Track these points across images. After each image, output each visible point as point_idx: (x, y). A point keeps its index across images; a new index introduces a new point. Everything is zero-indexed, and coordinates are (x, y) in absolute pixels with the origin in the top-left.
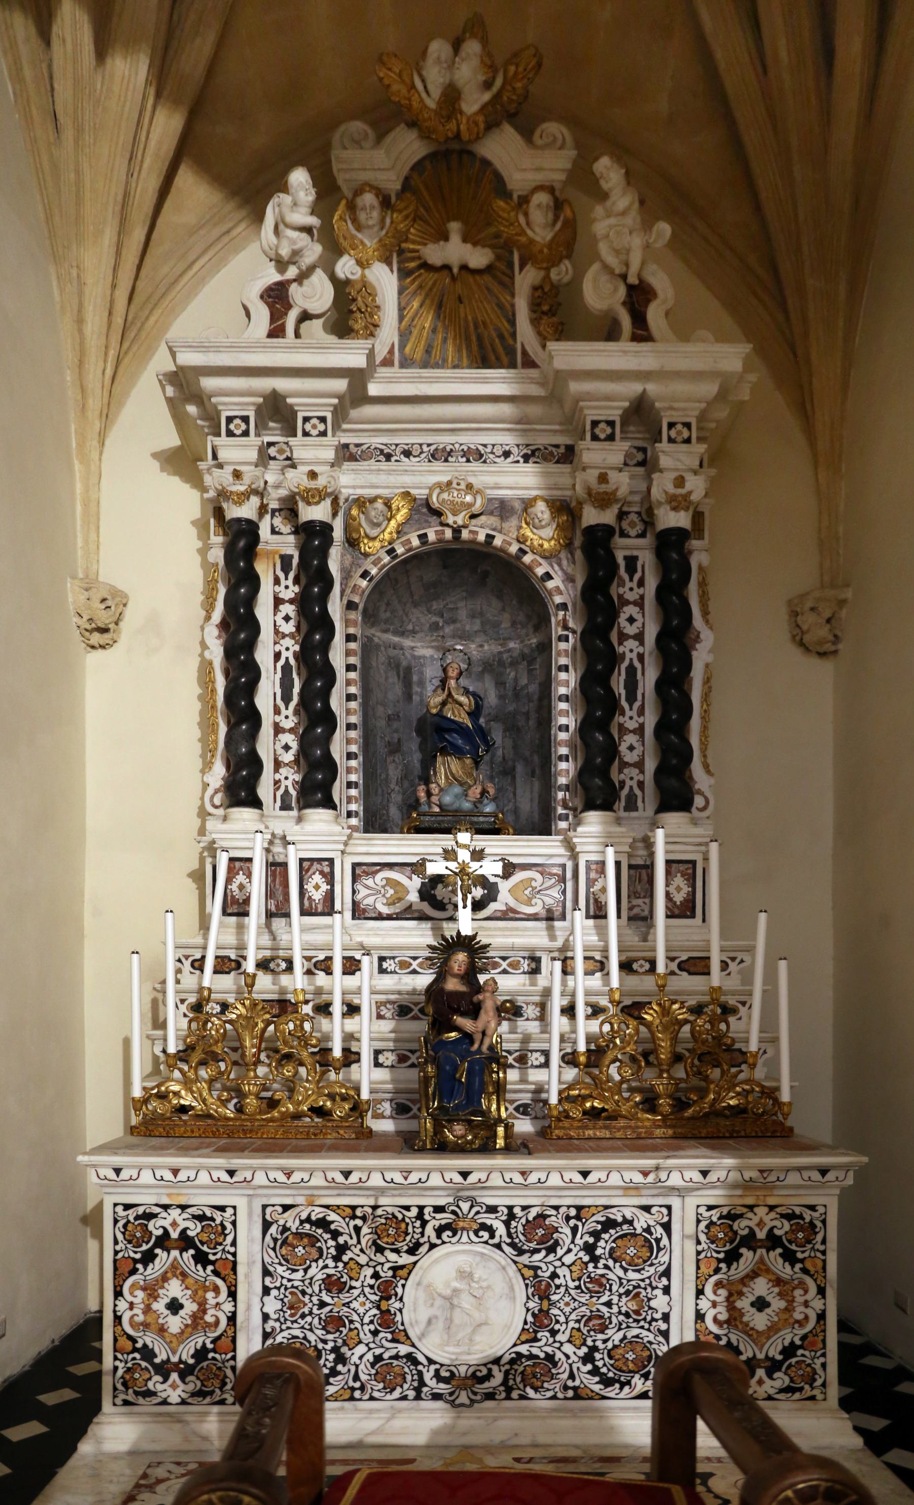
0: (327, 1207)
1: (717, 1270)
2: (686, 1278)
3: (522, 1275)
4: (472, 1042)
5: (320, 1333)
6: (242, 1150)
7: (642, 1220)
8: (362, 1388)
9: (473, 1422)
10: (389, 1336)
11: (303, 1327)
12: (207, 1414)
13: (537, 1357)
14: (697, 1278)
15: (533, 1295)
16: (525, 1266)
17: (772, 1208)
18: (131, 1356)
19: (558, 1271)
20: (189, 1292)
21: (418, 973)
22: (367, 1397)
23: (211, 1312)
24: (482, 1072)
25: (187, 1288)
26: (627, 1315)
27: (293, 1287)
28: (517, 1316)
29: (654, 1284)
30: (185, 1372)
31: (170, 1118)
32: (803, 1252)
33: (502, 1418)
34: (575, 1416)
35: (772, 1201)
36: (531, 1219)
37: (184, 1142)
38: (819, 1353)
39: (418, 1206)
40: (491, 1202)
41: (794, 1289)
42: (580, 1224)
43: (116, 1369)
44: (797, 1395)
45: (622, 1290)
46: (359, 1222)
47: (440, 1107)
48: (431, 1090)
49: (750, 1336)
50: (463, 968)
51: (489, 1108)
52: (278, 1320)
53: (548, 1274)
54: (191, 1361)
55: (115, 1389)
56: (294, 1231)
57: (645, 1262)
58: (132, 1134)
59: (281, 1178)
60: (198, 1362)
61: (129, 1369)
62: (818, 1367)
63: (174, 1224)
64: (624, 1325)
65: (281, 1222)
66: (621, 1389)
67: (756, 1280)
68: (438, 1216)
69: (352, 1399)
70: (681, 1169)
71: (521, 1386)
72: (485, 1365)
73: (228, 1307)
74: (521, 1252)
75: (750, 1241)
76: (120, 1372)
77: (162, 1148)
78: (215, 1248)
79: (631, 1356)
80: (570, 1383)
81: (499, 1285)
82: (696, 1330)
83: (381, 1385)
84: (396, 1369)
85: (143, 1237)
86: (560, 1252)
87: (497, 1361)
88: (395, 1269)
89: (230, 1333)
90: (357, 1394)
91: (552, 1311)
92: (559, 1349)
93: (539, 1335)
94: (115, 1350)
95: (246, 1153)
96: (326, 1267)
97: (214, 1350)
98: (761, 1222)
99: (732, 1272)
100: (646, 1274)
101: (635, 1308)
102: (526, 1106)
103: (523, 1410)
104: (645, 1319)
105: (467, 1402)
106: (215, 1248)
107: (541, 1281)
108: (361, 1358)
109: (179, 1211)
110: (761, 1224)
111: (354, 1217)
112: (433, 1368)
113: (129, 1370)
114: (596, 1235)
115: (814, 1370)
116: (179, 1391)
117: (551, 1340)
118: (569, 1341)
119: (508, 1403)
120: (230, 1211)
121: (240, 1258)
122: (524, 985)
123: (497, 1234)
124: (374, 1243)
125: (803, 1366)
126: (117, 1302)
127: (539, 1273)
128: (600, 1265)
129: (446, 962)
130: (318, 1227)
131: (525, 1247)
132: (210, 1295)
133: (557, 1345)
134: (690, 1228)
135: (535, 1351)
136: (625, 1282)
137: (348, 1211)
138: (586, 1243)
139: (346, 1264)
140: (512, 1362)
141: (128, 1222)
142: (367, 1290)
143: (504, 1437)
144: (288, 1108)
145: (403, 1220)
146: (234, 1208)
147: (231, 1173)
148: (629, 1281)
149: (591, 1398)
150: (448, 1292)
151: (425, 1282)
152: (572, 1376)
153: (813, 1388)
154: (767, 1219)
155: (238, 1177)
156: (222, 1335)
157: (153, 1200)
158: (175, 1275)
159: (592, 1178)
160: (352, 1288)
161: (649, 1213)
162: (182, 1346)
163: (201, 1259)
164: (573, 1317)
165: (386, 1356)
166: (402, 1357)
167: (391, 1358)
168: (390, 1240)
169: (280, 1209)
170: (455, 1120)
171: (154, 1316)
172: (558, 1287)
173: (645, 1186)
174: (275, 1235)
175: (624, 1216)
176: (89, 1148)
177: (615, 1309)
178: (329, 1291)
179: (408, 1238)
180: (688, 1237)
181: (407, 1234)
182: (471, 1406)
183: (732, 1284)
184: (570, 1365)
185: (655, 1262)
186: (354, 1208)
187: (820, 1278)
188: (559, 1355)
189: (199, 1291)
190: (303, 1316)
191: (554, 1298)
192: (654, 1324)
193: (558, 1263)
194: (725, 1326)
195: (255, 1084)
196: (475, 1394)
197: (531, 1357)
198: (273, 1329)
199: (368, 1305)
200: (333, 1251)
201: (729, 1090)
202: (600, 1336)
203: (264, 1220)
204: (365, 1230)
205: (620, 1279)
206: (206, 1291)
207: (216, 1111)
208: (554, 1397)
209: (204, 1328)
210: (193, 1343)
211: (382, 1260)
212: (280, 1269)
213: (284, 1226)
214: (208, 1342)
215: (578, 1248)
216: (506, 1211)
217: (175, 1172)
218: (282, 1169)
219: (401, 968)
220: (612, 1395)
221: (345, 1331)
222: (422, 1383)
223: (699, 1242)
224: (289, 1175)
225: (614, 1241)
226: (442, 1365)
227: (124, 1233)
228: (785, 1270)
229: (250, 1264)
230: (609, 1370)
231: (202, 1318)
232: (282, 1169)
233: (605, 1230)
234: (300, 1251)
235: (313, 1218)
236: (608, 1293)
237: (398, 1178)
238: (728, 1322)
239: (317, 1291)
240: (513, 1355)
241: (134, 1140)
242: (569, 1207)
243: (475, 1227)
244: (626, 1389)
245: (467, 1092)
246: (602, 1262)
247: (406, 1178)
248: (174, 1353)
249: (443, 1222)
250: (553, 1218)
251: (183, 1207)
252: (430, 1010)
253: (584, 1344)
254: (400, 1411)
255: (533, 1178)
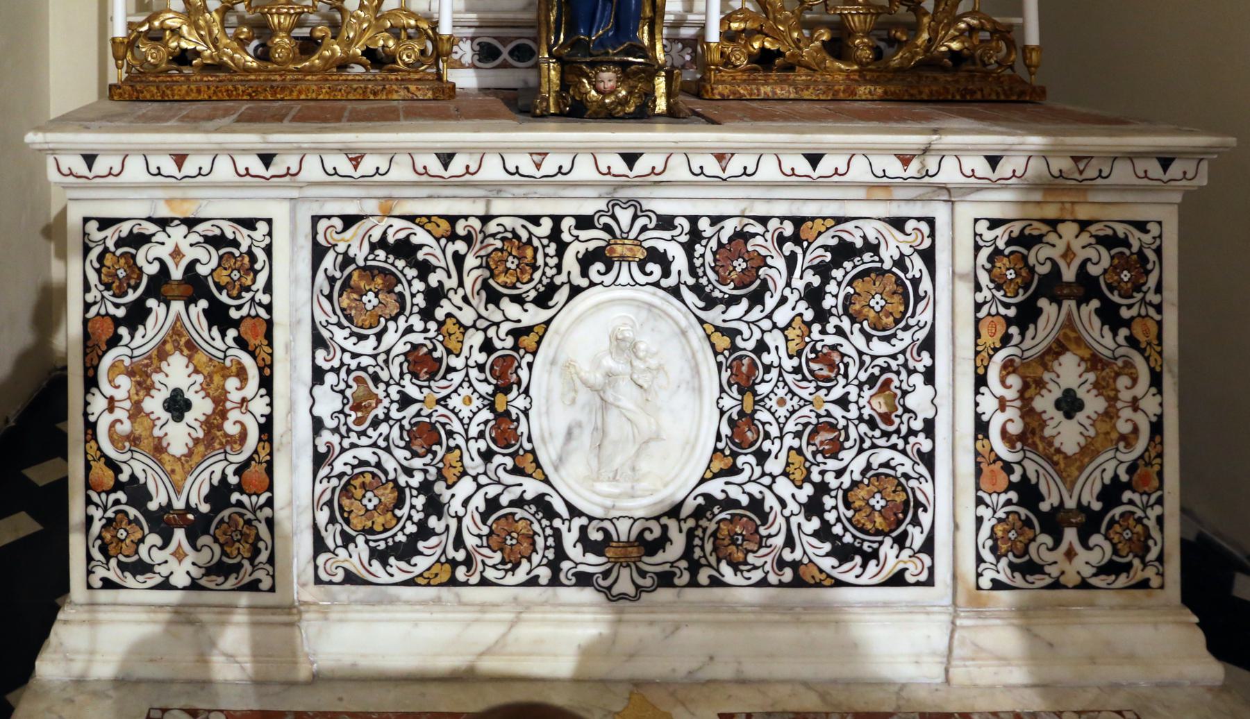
0: (411, 218)
1: (1006, 340)
2: (958, 354)
3: (713, 346)
5: (401, 454)
6: (278, 118)
7: (892, 244)
8: (468, 562)
9: (643, 631)
10: (509, 462)
11: (375, 445)
12: (230, 608)
13: (736, 504)
14: (977, 353)
15: (730, 385)
16: (717, 329)
17: (1084, 225)
18: (113, 497)
19: (768, 338)
20: (199, 378)
22: (475, 579)
23: (234, 415)
25: (196, 371)
26: (872, 424)
27: (359, 368)
28: (705, 423)
29: (911, 364)
30: (197, 527)
31: (166, 71)
32: (1130, 307)
33: (687, 624)
34: (798, 622)
35: (1083, 213)
36: (725, 240)
37: (188, 109)
38: (1154, 498)
39: (552, 217)
40: (664, 208)
41: (1118, 375)
42: (799, 250)
43: (89, 520)
44: (1123, 580)
45: (863, 376)
46: (461, 246)
49: (1054, 464)
52: (336, 430)
53: (751, 344)
54: (205, 508)
55: (89, 558)
56: (361, 263)
57: (897, 322)
58: (111, 97)
59: (345, 167)
60: (215, 510)
61: (110, 521)
62: (1151, 523)
63: (177, 254)
64: (867, 444)
65: (341, 248)
66: (864, 566)
67: (1062, 359)
68: (584, 234)
69: (453, 582)
70: (958, 153)
71: (713, 560)
72: (657, 518)
73: (259, 406)
74: (710, 303)
75: (1051, 286)
76: (96, 527)
77: (158, 119)
78: (239, 297)
79: (878, 502)
80: (788, 556)
81: (677, 366)
82: (977, 454)
83: (498, 557)
84: (521, 524)
85: (128, 277)
86: (770, 302)
87: (674, 511)
88: (517, 333)
89: (263, 454)
90: (461, 573)
91: (758, 416)
92: (770, 487)
93: (740, 460)
94: (88, 486)
95: (286, 123)
96: (410, 330)
97: (239, 488)
98: (1068, 250)
99: (1028, 343)
100: (900, 346)
101: (883, 409)
103: (716, 607)
104: (898, 431)
105: (631, 590)
106: (239, 297)
107: (741, 358)
108: (465, 503)
109: (183, 229)
110: (1068, 253)
111: (453, 237)
112: (578, 522)
113: (110, 521)
114: (823, 270)
115: (1146, 528)
116: (187, 565)
117: (758, 471)
118: (785, 474)
119: (693, 594)
120: (262, 228)
121: (279, 315)
123: (674, 268)
124: (485, 285)
125: (1131, 522)
126: (89, 398)
127: (739, 342)
128: (830, 328)
130: (397, 257)
131: (717, 294)
132: (232, 383)
133: (767, 480)
134: (965, 261)
135: (734, 492)
136: (867, 359)
137: (445, 225)
138: (809, 285)
139: (441, 324)
140: (699, 513)
141: (106, 250)
142: (474, 373)
143: (694, 665)
144: (333, 51)
145: (529, 242)
146: (269, 221)
147: (267, 159)
148: (874, 358)
149: (819, 585)
150: (597, 378)
151: (562, 360)
152: (790, 543)
153: (1145, 565)
154: (1076, 245)
155: (278, 167)
156: (251, 458)
157: (143, 210)
158: (177, 348)
159: (825, 167)
160: (450, 369)
161: (902, 231)
162: (190, 479)
163: (218, 317)
164: (791, 426)
165: (504, 500)
166: (529, 503)
167: (512, 504)
168: (510, 279)
169: (339, 224)
170: (602, 63)
171: (147, 423)
172: (767, 369)
173: (904, 183)
174: (331, 272)
175: (864, 237)
176: (55, 111)
177: (853, 413)
178: (415, 375)
179: (537, 276)
180: (963, 277)
181: (535, 268)
182: (636, 598)
183: (1028, 365)
184: (787, 519)
185: (912, 322)
186: (452, 220)
187: (1155, 356)
188: (770, 502)
189: (216, 373)
190: (375, 424)
191: (762, 389)
192: (912, 440)
193: (766, 324)
194: (1019, 445)
195: (288, 14)
196: (643, 574)
197: (730, 503)
198: (330, 446)
199: (477, 403)
200: (420, 300)
201: (948, 26)
202: (833, 464)
203: (315, 243)
204: (471, 262)
205: (860, 353)
206: (225, 377)
207: (232, 58)
208: (763, 583)
209: (223, 445)
210: (206, 474)
211: (497, 317)
212: (340, 335)
213: (346, 254)
214: (230, 471)
215: (796, 295)
216: (687, 226)
217: (180, 159)
218: (346, 151)
220: (849, 578)
221: (440, 451)
222: (561, 555)
223: (978, 288)
224: (356, 162)
225: (850, 284)
226: (591, 519)
227: (98, 271)
228: (1104, 341)
229: (295, 324)
230: (846, 530)
231: (220, 428)
232: (346, 151)
233: (836, 263)
234: (370, 300)
235: (391, 239)
236: (842, 381)
237: (527, 167)
238: (1022, 437)
239: (397, 377)
240: (700, 500)
241: (116, 107)
242: (782, 219)
243: (641, 255)
244: (872, 566)
246: (834, 321)
247: (538, 166)
248: (178, 492)
249: (592, 246)
250: (759, 240)
251: (191, 223)
253: (807, 479)
254: (528, 607)
255: (735, 167)
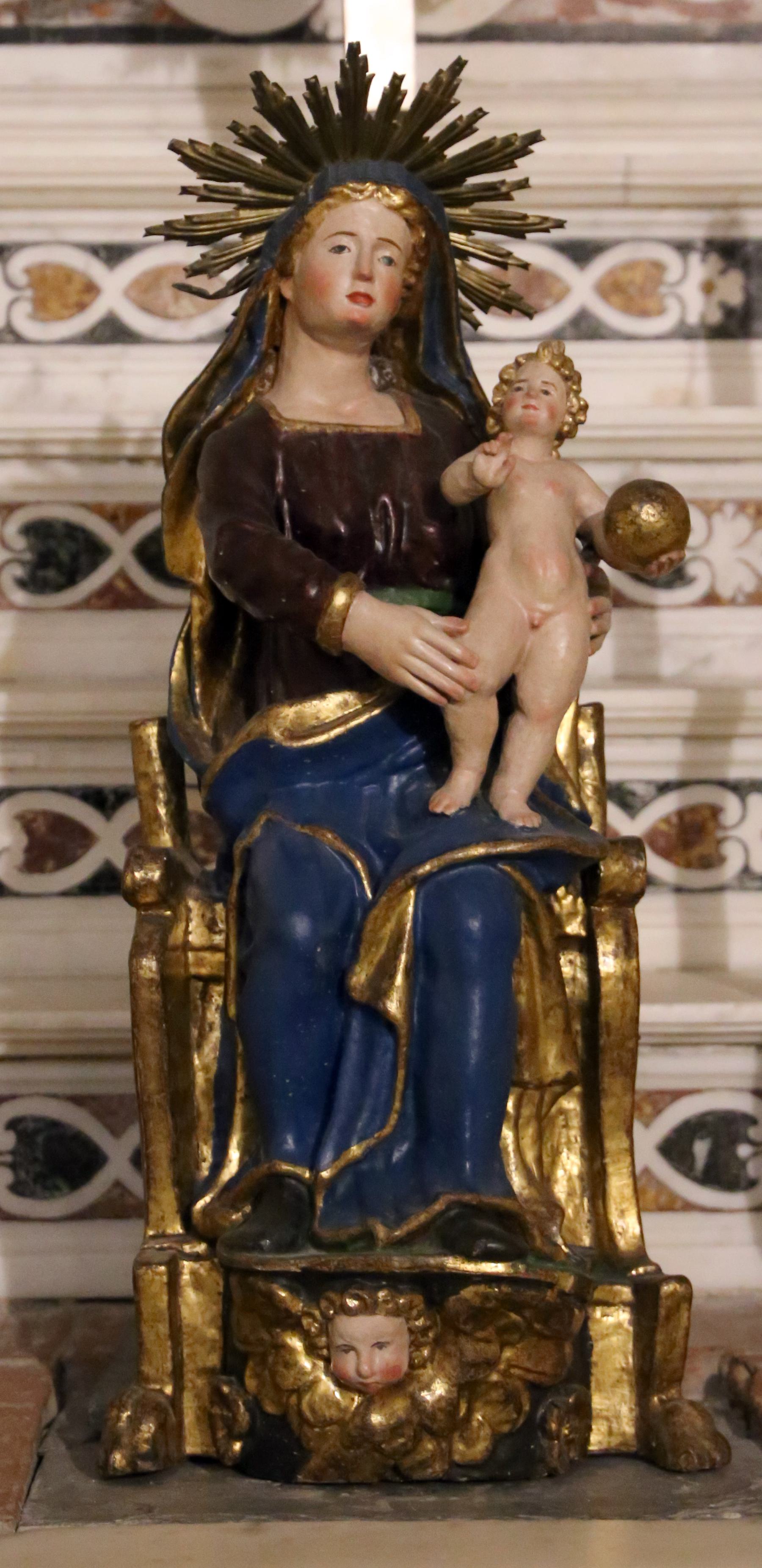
4: (440, 759)
21: (95, 250)
24: (503, 947)
47: (261, 1188)
48: (205, 1060)
50: (384, 284)
51: (542, 1181)
102: (722, 1127)
122: (687, 400)
129: (281, 247)
170: (346, 1280)
219: (42, 309)
245: (418, 1082)
252: (193, 550)
